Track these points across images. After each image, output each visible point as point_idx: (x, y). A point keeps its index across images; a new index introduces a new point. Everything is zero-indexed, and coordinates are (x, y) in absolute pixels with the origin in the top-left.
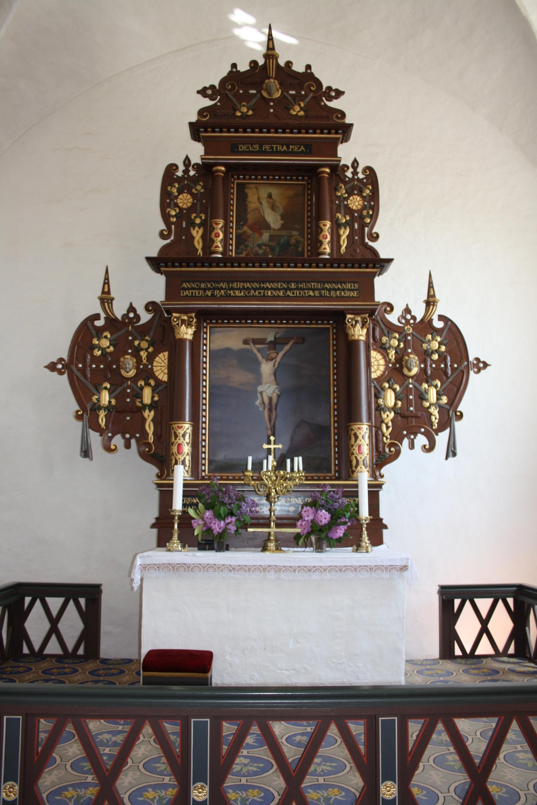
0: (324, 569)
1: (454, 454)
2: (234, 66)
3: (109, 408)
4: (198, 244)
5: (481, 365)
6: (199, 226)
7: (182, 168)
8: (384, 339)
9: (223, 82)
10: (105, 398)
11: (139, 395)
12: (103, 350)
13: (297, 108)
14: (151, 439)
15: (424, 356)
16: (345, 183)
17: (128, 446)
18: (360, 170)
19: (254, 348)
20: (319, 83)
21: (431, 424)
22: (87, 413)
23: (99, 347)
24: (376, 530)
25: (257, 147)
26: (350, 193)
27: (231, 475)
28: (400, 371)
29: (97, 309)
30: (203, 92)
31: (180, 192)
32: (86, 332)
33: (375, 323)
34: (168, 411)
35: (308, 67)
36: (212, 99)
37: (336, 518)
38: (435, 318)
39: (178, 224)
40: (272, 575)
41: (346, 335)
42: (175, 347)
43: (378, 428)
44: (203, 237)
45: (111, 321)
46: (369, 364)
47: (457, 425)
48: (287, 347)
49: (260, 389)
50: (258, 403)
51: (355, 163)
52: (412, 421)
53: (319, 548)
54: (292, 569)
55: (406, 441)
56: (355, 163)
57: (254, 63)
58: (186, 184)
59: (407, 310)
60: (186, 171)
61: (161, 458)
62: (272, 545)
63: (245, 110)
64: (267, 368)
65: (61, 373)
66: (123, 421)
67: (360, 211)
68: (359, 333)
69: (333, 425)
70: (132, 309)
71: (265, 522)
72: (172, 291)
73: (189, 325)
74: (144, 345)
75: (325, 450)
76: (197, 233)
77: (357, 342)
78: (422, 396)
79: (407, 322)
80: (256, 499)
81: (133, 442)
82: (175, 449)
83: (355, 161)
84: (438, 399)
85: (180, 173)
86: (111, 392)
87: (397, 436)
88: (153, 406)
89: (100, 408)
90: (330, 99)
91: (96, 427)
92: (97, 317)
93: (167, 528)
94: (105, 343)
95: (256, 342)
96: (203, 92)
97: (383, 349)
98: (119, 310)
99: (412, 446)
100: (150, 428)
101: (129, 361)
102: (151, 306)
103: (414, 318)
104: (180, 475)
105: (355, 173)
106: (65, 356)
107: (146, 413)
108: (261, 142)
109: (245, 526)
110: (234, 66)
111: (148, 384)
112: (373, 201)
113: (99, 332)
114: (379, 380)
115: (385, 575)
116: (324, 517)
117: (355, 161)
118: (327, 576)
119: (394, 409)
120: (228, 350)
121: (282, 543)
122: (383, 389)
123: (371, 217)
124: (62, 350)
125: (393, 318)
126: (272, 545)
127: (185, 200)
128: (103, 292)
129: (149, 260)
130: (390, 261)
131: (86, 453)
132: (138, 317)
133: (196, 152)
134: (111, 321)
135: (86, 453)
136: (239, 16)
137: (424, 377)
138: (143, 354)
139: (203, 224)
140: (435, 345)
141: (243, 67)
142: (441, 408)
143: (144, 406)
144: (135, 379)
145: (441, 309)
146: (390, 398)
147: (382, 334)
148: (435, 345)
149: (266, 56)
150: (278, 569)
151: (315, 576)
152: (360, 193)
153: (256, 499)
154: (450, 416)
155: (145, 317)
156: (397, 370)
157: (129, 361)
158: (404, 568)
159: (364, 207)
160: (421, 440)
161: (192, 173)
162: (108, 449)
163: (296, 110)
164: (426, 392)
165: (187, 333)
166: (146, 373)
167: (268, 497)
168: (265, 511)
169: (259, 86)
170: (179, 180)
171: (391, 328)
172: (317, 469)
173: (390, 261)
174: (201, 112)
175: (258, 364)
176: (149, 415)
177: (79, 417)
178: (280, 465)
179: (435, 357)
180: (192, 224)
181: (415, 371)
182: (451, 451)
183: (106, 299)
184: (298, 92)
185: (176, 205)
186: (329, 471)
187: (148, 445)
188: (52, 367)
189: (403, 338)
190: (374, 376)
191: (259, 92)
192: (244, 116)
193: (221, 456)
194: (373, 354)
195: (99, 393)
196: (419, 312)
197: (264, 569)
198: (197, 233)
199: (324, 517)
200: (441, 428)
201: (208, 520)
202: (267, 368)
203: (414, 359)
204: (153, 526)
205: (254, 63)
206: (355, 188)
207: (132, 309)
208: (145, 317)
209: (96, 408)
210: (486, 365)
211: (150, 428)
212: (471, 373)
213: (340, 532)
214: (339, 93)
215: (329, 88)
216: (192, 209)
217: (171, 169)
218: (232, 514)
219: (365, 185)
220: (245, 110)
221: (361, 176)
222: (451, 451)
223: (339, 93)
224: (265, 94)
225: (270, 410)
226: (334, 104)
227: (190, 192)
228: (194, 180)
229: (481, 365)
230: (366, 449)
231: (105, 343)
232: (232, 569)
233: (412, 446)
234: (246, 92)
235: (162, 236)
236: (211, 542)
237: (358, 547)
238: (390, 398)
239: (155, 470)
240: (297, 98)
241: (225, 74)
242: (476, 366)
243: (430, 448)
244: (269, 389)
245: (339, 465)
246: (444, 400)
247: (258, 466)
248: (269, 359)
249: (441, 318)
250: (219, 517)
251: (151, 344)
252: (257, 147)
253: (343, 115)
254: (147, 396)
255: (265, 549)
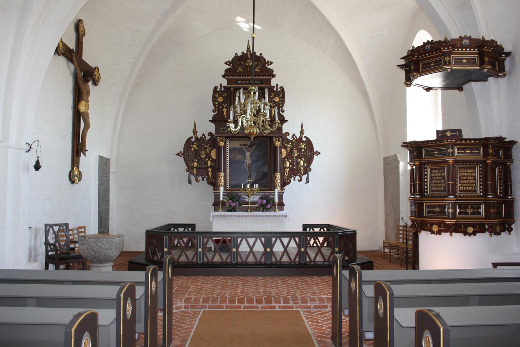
0: (264, 216)
1: (308, 182)
2: (236, 54)
3: (197, 168)
4: (225, 114)
5: (318, 153)
6: (226, 108)
7: (219, 87)
8: (286, 145)
9: (233, 60)
10: (195, 164)
11: (207, 164)
12: (194, 149)
13: (257, 69)
14: (211, 177)
15: (299, 150)
16: (274, 92)
17: (203, 180)
18: (278, 88)
19: (243, 147)
20: (265, 60)
21: (301, 172)
22: (190, 169)
23: (193, 148)
24: (281, 205)
25: (244, 82)
26: (275, 96)
27: (236, 189)
28: (291, 155)
29: (192, 135)
30: (226, 63)
31: (219, 96)
32: (189, 142)
33: (283, 139)
34: (216, 169)
35: (261, 54)
36: (229, 65)
37: (268, 203)
38: (303, 137)
39: (218, 107)
40: (249, 218)
41: (274, 144)
42: (218, 149)
43: (284, 174)
44: (227, 112)
45: (197, 139)
46: (281, 153)
47: (309, 173)
48: (254, 147)
49: (246, 161)
50: (245, 165)
51: (277, 85)
52: (295, 172)
53: (263, 211)
54: (255, 216)
55: (293, 178)
56: (277, 85)
57: (243, 53)
58: (221, 93)
59: (294, 135)
60: (221, 89)
61: (214, 184)
62: (249, 210)
63: (240, 69)
64: (248, 154)
65: (181, 156)
66: (201, 172)
67: (278, 102)
68: (278, 144)
69: (269, 173)
70: (203, 135)
71: (247, 203)
72: (217, 130)
73: (223, 141)
74: (208, 147)
75: (266, 182)
76: (225, 110)
77: (277, 146)
78: (298, 163)
79: (294, 138)
80: (244, 196)
81: (205, 178)
82: (219, 181)
83: (277, 84)
84: (303, 164)
85: (218, 90)
86: (197, 162)
87: (290, 177)
88: (211, 167)
89: (194, 168)
90: (269, 65)
91: (193, 174)
92: (192, 137)
93: (217, 205)
94: (195, 146)
95: (244, 145)
96: (226, 63)
97: (286, 148)
98: (199, 135)
99: (294, 180)
100: (210, 174)
101: (203, 152)
102: (210, 134)
103: (296, 137)
104: (222, 189)
105: (277, 89)
106: (182, 151)
107: (209, 169)
108: (246, 80)
109: (241, 205)
110: (236, 54)
111: (209, 160)
112: (283, 99)
113: (193, 144)
114: (284, 158)
115: (281, 218)
116: (264, 202)
117: (277, 84)
118: (264, 218)
119: (289, 167)
120: (235, 148)
121: (252, 210)
122: (286, 161)
123: (282, 104)
124: (181, 148)
125: (289, 137)
126: (249, 210)
127: (220, 99)
128: (194, 130)
129: (210, 121)
130: (287, 121)
131: (190, 182)
132: (205, 138)
133: (224, 82)
134: (197, 139)
135: (190, 182)
136: (239, 19)
137: (299, 157)
138: (208, 150)
139: (227, 107)
140: (303, 146)
141: (240, 54)
142: (304, 168)
143: (208, 167)
144: (205, 158)
145: (305, 135)
146: (288, 164)
147: (286, 143)
148: (303, 146)
149: (247, 51)
150: (251, 216)
151: (261, 218)
152: (278, 96)
153: (244, 196)
154: (307, 170)
155: (208, 138)
156: (290, 155)
157: (203, 152)
158: (286, 216)
159: (280, 101)
160: (298, 178)
161: (223, 89)
162: (197, 181)
163: (257, 70)
164: (300, 162)
165: (222, 144)
166: (209, 156)
167: (248, 196)
168: (247, 200)
169: (245, 61)
170: (219, 92)
171: (288, 141)
172: (265, 187)
173: (287, 121)
174: (226, 71)
175: (245, 153)
176: (210, 170)
177: (187, 171)
178: (252, 186)
179: (303, 150)
180: (223, 107)
181: (296, 155)
182: (307, 181)
183: (195, 132)
184: (258, 63)
185: (218, 101)
186: (268, 187)
187: (210, 179)
188: (178, 154)
189: (292, 144)
190: (282, 157)
191: (245, 63)
192: (240, 72)
193: (233, 183)
194: (282, 150)
195: (194, 163)
196: (298, 135)
197: (247, 216)
198: (225, 110)
199: (264, 202)
200: (304, 174)
201: (233, 203)
202: (248, 154)
203: (296, 151)
204: (213, 205)
205: (243, 53)
206: (277, 94)
207: (203, 135)
208: (208, 138)
209: (193, 167)
210: (319, 153)
211: (210, 174)
212: (315, 156)
213: (269, 206)
214: (271, 63)
215: (268, 61)
216: (223, 102)
217: (216, 88)
218: (237, 201)
219: (280, 93)
220: (240, 69)
221: (279, 90)
222: (307, 181)
223: (271, 63)
224: (247, 64)
225: (249, 168)
226: (270, 67)
227: (222, 96)
228: (223, 92)
229: (318, 153)
230: (279, 181)
231: (195, 146)
232: (238, 216)
233: (294, 180)
234: (240, 63)
235: (214, 111)
236: (232, 209)
237: (275, 211)
238: (288, 164)
239: (213, 188)
240: (258, 65)
241: (233, 57)
242: (316, 153)
243: (300, 181)
244: (248, 161)
245: (271, 186)
246: (305, 165)
247: (245, 186)
248: (248, 151)
249: (305, 137)
250: (234, 202)
251: (210, 146)
252: (244, 82)
253: (273, 71)
254: (209, 163)
255: (247, 211)
